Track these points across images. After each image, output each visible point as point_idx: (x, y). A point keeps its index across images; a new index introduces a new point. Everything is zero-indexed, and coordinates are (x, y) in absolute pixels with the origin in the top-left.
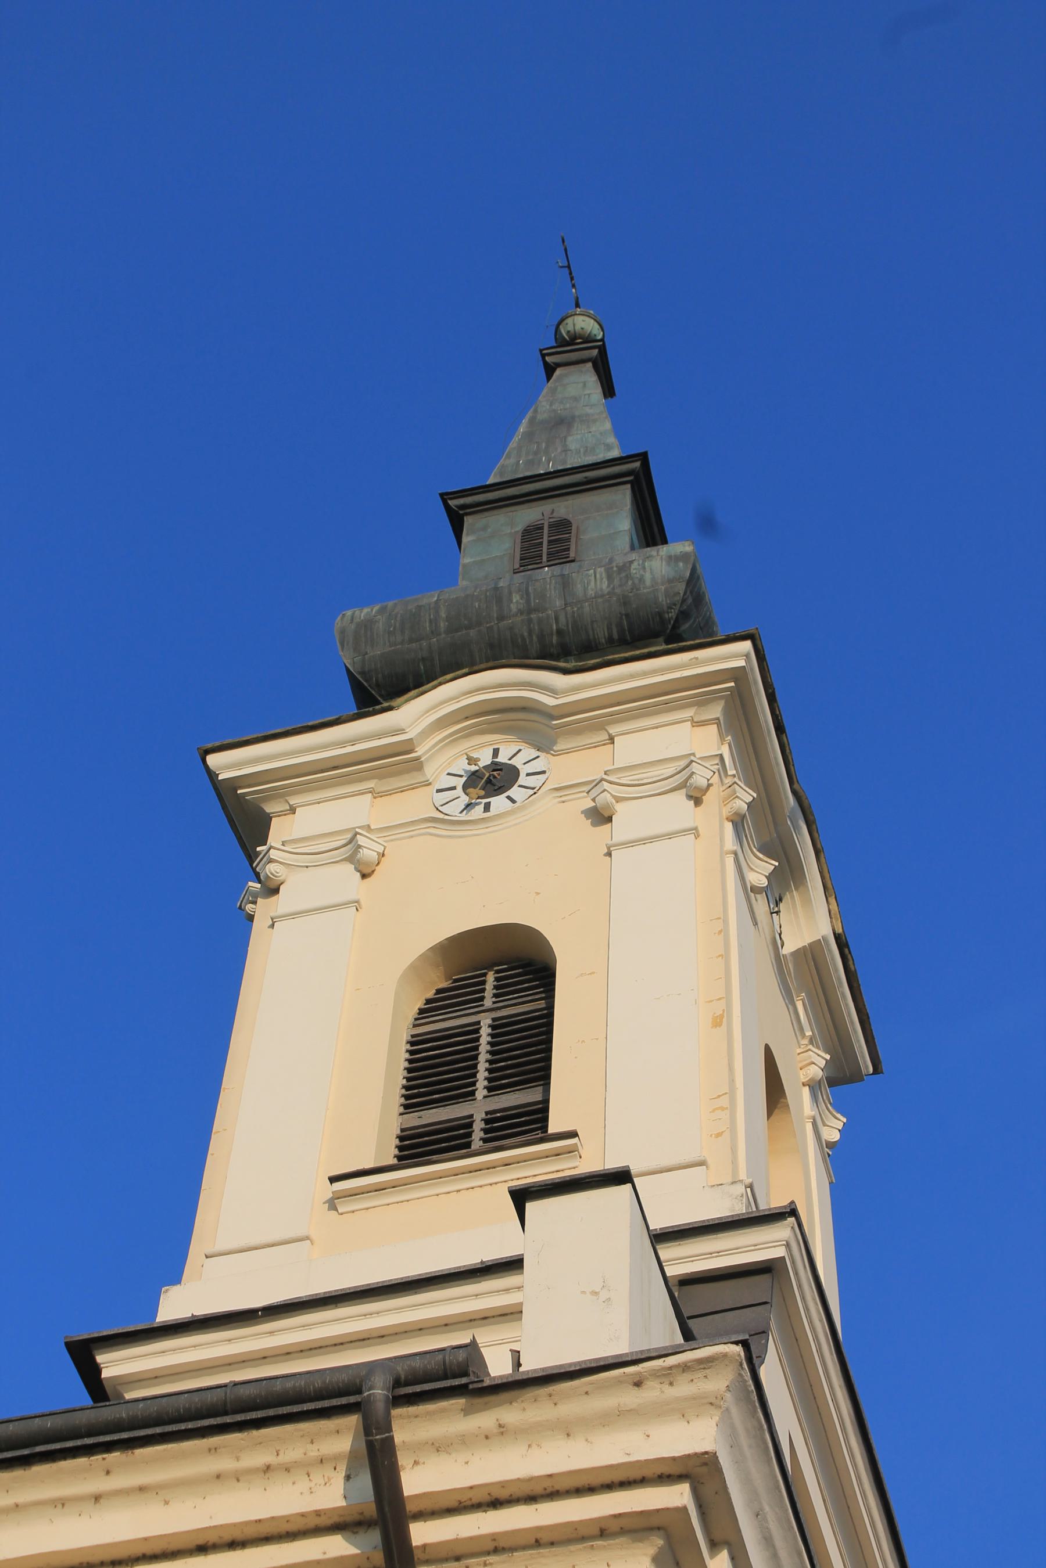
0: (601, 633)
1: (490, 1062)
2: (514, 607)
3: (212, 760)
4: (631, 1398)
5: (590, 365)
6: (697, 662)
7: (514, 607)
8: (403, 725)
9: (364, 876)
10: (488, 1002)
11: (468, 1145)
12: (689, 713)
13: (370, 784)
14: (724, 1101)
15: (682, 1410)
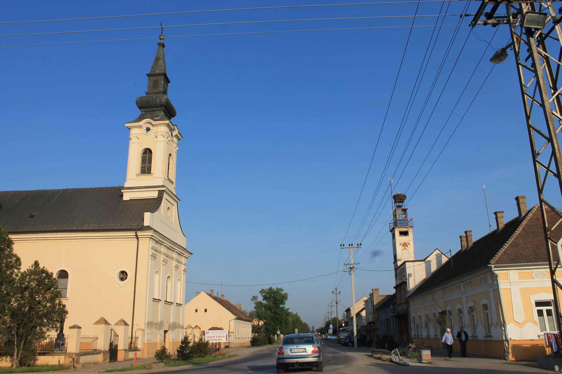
0: (159, 106)
3: (125, 124)
6: (164, 122)
15: (151, 232)
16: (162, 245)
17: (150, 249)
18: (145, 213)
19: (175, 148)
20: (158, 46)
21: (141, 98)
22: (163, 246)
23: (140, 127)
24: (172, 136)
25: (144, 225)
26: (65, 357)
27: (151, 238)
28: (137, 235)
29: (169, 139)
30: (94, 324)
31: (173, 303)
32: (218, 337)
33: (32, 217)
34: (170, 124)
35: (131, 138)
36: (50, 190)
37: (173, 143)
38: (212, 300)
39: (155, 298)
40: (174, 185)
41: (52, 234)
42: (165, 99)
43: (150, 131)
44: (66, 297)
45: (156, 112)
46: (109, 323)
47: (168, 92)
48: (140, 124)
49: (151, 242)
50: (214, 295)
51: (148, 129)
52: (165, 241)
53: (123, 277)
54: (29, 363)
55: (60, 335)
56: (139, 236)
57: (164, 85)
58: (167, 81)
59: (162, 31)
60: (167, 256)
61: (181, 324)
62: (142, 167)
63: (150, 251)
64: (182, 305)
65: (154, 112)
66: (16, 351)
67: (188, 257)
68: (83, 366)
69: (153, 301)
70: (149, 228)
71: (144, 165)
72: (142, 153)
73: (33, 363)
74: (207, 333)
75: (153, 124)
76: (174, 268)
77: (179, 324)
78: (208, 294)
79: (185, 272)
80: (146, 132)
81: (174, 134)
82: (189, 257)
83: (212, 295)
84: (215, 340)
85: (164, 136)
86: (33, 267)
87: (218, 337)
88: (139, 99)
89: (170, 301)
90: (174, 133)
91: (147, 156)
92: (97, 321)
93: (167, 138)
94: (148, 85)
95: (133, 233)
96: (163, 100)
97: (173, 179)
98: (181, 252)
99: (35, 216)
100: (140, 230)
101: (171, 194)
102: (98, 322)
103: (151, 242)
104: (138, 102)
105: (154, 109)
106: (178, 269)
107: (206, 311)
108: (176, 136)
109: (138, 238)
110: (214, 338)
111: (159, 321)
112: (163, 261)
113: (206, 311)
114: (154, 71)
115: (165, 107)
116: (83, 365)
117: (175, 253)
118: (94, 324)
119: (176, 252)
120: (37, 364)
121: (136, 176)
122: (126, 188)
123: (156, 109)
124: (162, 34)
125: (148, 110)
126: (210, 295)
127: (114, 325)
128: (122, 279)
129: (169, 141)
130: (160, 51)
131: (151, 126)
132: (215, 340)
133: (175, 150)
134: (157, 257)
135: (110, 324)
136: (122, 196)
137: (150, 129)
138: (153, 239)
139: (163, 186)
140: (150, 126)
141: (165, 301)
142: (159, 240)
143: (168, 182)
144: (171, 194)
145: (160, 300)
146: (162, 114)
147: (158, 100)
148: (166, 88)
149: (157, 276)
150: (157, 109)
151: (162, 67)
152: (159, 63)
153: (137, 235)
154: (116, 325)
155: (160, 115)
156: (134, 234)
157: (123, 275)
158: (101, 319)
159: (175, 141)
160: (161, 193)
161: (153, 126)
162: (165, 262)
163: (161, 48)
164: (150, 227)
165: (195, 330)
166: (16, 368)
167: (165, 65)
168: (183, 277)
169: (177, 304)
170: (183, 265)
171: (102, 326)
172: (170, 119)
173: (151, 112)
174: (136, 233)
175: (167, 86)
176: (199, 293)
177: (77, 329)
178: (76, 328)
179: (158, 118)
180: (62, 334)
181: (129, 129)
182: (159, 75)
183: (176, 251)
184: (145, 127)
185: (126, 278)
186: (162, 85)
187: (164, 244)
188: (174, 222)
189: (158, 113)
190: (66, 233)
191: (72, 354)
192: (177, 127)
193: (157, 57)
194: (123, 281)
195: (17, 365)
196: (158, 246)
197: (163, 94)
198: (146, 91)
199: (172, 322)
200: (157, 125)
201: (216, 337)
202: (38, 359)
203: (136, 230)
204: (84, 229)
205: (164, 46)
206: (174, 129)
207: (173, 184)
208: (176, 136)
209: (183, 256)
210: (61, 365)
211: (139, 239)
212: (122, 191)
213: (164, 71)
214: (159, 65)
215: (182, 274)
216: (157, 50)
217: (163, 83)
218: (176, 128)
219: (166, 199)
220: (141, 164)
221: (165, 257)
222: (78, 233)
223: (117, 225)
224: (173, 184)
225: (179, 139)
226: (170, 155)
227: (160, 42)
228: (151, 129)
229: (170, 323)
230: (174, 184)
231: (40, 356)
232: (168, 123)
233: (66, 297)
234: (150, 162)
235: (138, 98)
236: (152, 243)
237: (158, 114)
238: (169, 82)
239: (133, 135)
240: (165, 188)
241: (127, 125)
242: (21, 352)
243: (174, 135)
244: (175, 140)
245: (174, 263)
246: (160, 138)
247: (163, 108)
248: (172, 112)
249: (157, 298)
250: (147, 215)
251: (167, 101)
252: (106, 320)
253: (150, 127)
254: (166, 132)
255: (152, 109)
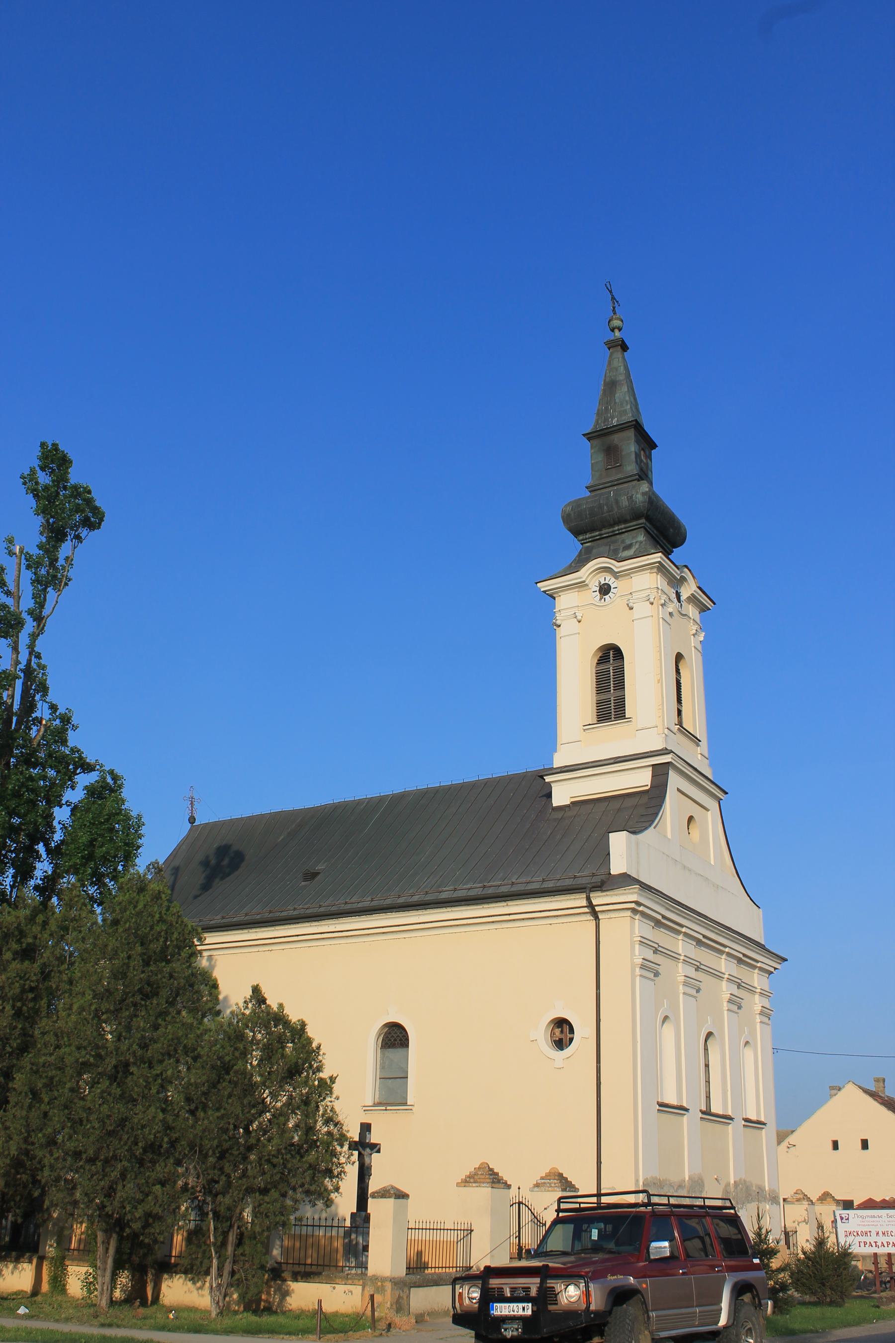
0: (628, 518)
1: (614, 687)
2: (605, 511)
4: (625, 892)
5: (619, 347)
6: (648, 559)
7: (605, 511)
8: (582, 576)
9: (579, 622)
10: (611, 661)
11: (611, 718)
12: (649, 571)
13: (577, 590)
14: (660, 707)
15: (632, 893)
16: (678, 932)
17: (637, 946)
18: (612, 836)
19: (694, 635)
20: (609, 349)
21: (577, 503)
22: (681, 937)
23: (581, 585)
24: (679, 600)
25: (612, 873)
26: (363, 1290)
27: (634, 911)
28: (591, 906)
29: (670, 610)
30: (458, 1185)
31: (731, 1119)
32: (880, 1233)
33: (311, 876)
34: (667, 563)
35: (558, 622)
36: (359, 802)
37: (684, 621)
38: (883, 1110)
39: (666, 1101)
40: (704, 747)
41: (357, 919)
42: (644, 494)
43: (610, 594)
44: (405, 1104)
45: (623, 536)
46: (506, 1183)
47: (655, 475)
48: (581, 578)
49: (637, 921)
50: (886, 1094)
51: (605, 590)
52: (685, 918)
53: (562, 1036)
54: (269, 1302)
55: (358, 1219)
56: (597, 909)
57: (637, 455)
58: (647, 443)
59: (614, 308)
60: (697, 969)
61: (767, 1188)
62: (599, 703)
63: (637, 953)
64: (764, 1124)
65: (618, 536)
66: (215, 1261)
67: (772, 970)
68: (416, 1322)
69: (658, 1110)
70: (626, 880)
71: (603, 697)
72: (596, 661)
73: (278, 1304)
74: (842, 1218)
75: (616, 570)
76: (725, 1004)
77: (761, 1189)
78: (866, 1092)
79: (766, 1020)
80: (601, 599)
81: (685, 593)
82: (775, 969)
83: (880, 1094)
84: (874, 1245)
85: (652, 600)
86: (250, 1005)
87: (880, 1233)
88: (569, 509)
89: (721, 1112)
90: (687, 591)
91: (611, 668)
92: (470, 1176)
93: (663, 605)
94: (592, 464)
95: (579, 900)
96: (639, 496)
97: (700, 731)
98: (744, 955)
99: (318, 873)
100: (600, 887)
101: (692, 774)
102: (470, 1180)
103: (637, 921)
104: (569, 515)
105: (616, 528)
106: (698, 991)
107: (865, 1144)
108: (693, 599)
109: (595, 914)
110: (867, 1239)
111: (687, 1178)
112: (685, 984)
113: (865, 1144)
114: (606, 420)
115: (648, 518)
116: (420, 1319)
117: (724, 956)
118: (458, 1185)
119: (729, 954)
120: (290, 1308)
121: (584, 730)
122: (559, 770)
123: (623, 526)
124: (615, 313)
125: (600, 535)
126: (873, 1095)
127: (531, 1190)
128: (560, 1044)
129: (671, 614)
130: (615, 363)
131: (613, 579)
132: (874, 1245)
133: (695, 642)
134: (661, 969)
135: (509, 1187)
136: (549, 795)
137: (609, 586)
138: (643, 914)
139: (665, 752)
140: (610, 580)
141: (703, 1112)
142: (664, 917)
143: (681, 738)
144: (692, 774)
145: (687, 1110)
146: (641, 537)
147: (624, 502)
148: (647, 464)
149: (748, 1053)
150: (625, 528)
151: (627, 404)
152: (617, 395)
153: (591, 906)
154: (536, 1189)
155: (636, 542)
156: (584, 903)
157: (562, 1032)
158: (479, 1168)
159: (691, 616)
160: (660, 773)
161: (616, 578)
162: (694, 987)
163: (618, 353)
164: (629, 876)
165: (819, 1208)
166: (217, 1315)
167: (635, 399)
168: (761, 1033)
169: (746, 1120)
170: (757, 996)
171: (483, 1193)
172: (667, 553)
173: (609, 539)
174: (588, 899)
175: (649, 457)
176: (840, 1089)
177: (392, 1200)
178: (389, 1198)
179: (631, 552)
180: (363, 1214)
181: (551, 596)
182: (622, 428)
183: (727, 950)
184: (594, 586)
185: (571, 1040)
186: (633, 457)
187: (684, 930)
188: (712, 863)
189: (628, 538)
190: (394, 915)
191: (383, 1279)
192: (690, 571)
193: (607, 380)
194: (562, 1050)
195: (219, 1307)
196: (662, 938)
197: (639, 481)
198: (589, 481)
199: (732, 1182)
200: (628, 573)
201: (874, 1234)
202: (293, 1290)
203: (586, 889)
204: (443, 897)
205: (624, 347)
206: (683, 579)
207: (698, 745)
208: (693, 599)
209: (754, 967)
210: (325, 1315)
211: (601, 916)
212: (548, 779)
213: (633, 416)
214: (617, 401)
215: (758, 1026)
216: (606, 363)
217: (633, 449)
218: (687, 573)
219: (678, 790)
220: (595, 695)
221: (691, 972)
222: (425, 912)
223: (534, 879)
224: (698, 745)
225: (703, 609)
226: (679, 657)
227: (613, 338)
228: (612, 586)
229: (728, 1184)
230: (704, 743)
231: (297, 1281)
232: (659, 560)
233: (405, 1104)
234: (620, 685)
235: (566, 506)
236: (642, 928)
237: (628, 542)
238: (653, 446)
239: (563, 613)
240: (670, 756)
241: (544, 586)
242: (227, 1268)
243: (684, 597)
244: (692, 611)
245: (726, 989)
246: (642, 609)
247: (643, 521)
248: (671, 530)
249: (673, 1101)
250: (618, 842)
251: (650, 498)
252: (497, 1174)
253: (610, 583)
254: (658, 588)
255: (611, 530)
